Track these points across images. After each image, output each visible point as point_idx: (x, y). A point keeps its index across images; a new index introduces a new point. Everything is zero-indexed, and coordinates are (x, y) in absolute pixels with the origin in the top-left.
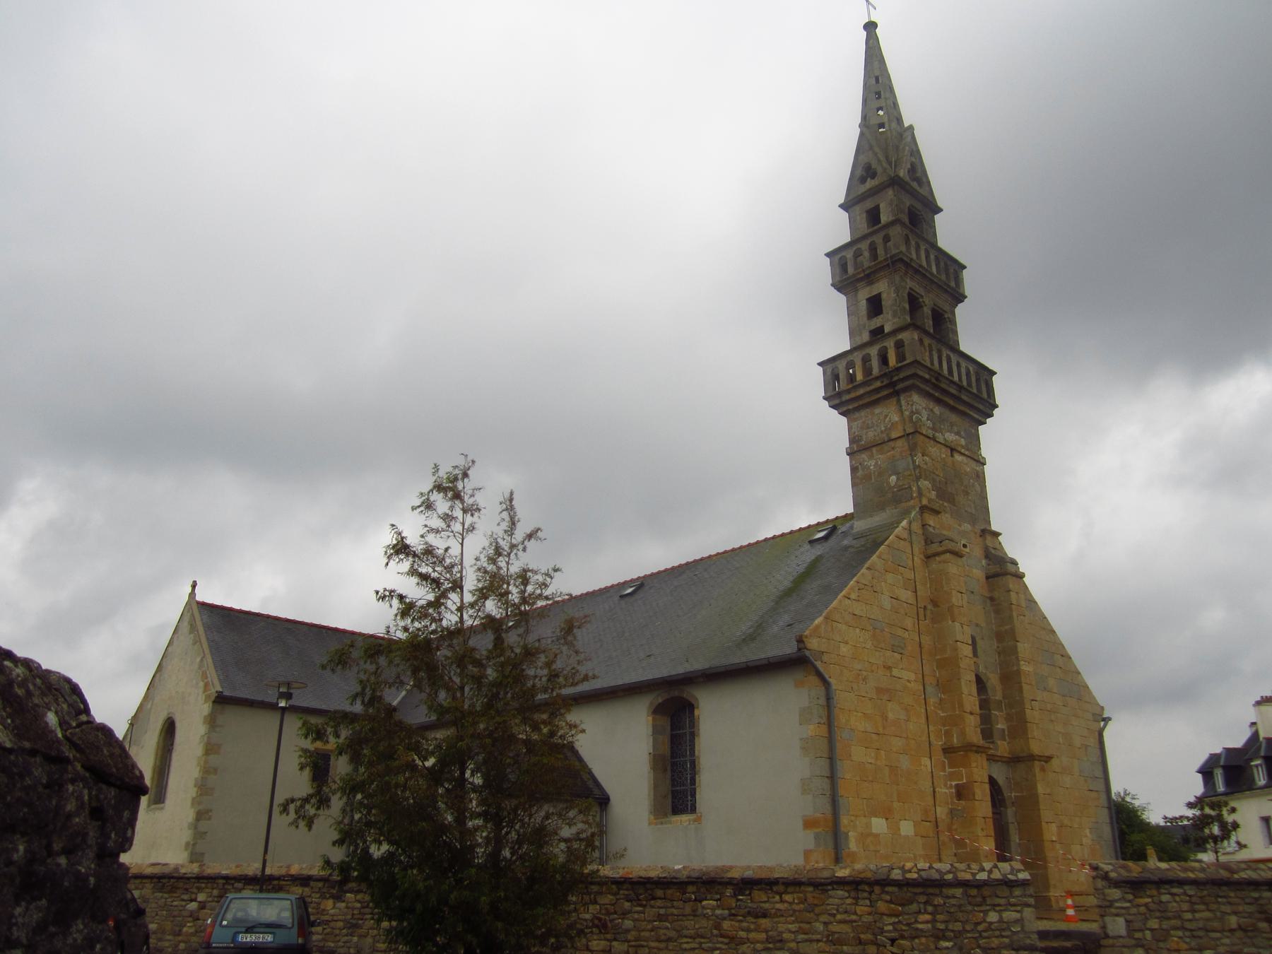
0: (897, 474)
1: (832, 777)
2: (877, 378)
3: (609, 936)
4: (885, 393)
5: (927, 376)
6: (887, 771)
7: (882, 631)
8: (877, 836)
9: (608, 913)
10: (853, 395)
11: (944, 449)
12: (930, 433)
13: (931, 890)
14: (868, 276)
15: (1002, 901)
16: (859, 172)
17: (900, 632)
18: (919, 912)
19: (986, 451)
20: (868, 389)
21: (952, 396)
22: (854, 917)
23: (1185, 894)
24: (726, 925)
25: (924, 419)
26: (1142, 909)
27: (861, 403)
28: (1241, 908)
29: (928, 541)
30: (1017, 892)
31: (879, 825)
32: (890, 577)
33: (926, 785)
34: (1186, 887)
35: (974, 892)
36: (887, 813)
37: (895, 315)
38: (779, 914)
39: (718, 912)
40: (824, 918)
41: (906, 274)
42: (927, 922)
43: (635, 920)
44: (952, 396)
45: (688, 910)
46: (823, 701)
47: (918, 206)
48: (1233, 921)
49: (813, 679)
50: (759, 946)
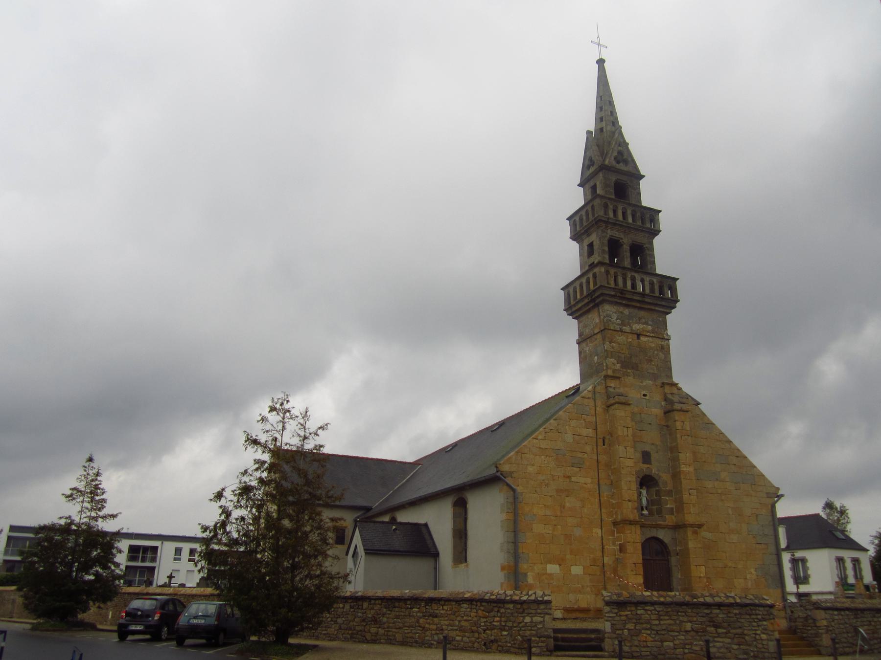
1: (515, 543)
2: (586, 297)
4: (591, 305)
5: (613, 293)
10: (577, 308)
11: (630, 336)
13: (500, 605)
15: (533, 611)
16: (587, 163)
24: (421, 621)
25: (614, 319)
26: (623, 618)
29: (609, 397)
30: (542, 607)
31: (553, 568)
35: (519, 606)
36: (560, 562)
38: (442, 616)
40: (459, 619)
41: (606, 227)
45: (407, 613)
46: (511, 500)
49: (505, 487)
50: (434, 632)
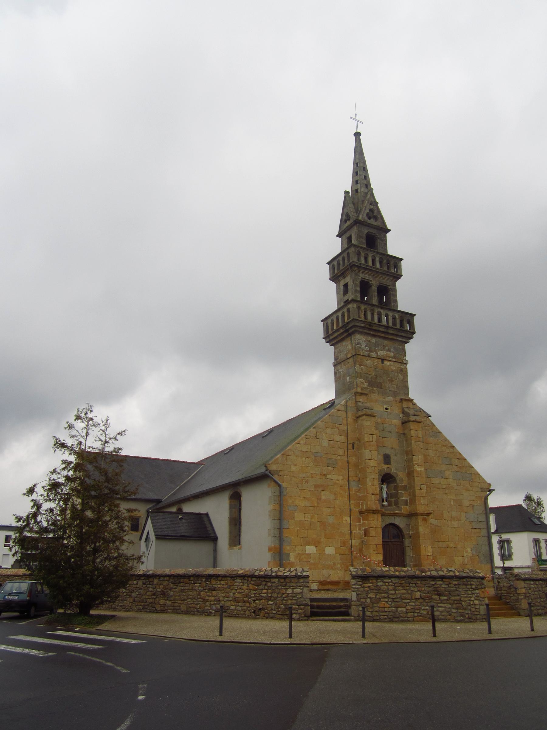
0: (349, 376)
2: (341, 328)
3: (166, 598)
4: (345, 335)
5: (363, 325)
6: (318, 524)
7: (322, 457)
8: (308, 554)
9: (166, 589)
11: (376, 360)
12: (366, 353)
14: (343, 274)
15: (294, 585)
16: (344, 217)
17: (334, 457)
18: (263, 589)
19: (408, 357)
20: (339, 333)
21: (383, 332)
22: (242, 591)
23: (392, 582)
24: (202, 593)
26: (367, 589)
27: (337, 340)
28: (423, 589)
30: (301, 581)
31: (310, 549)
32: (329, 431)
33: (346, 530)
34: (393, 579)
35: (282, 580)
36: (316, 543)
37: (352, 294)
39: (200, 588)
41: (359, 271)
42: (265, 593)
43: (174, 592)
44: (383, 332)
45: (190, 588)
46: (277, 493)
47: (374, 231)
48: (418, 595)
